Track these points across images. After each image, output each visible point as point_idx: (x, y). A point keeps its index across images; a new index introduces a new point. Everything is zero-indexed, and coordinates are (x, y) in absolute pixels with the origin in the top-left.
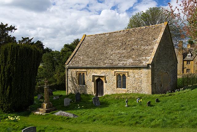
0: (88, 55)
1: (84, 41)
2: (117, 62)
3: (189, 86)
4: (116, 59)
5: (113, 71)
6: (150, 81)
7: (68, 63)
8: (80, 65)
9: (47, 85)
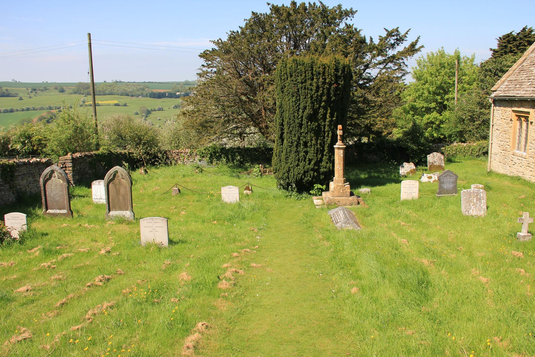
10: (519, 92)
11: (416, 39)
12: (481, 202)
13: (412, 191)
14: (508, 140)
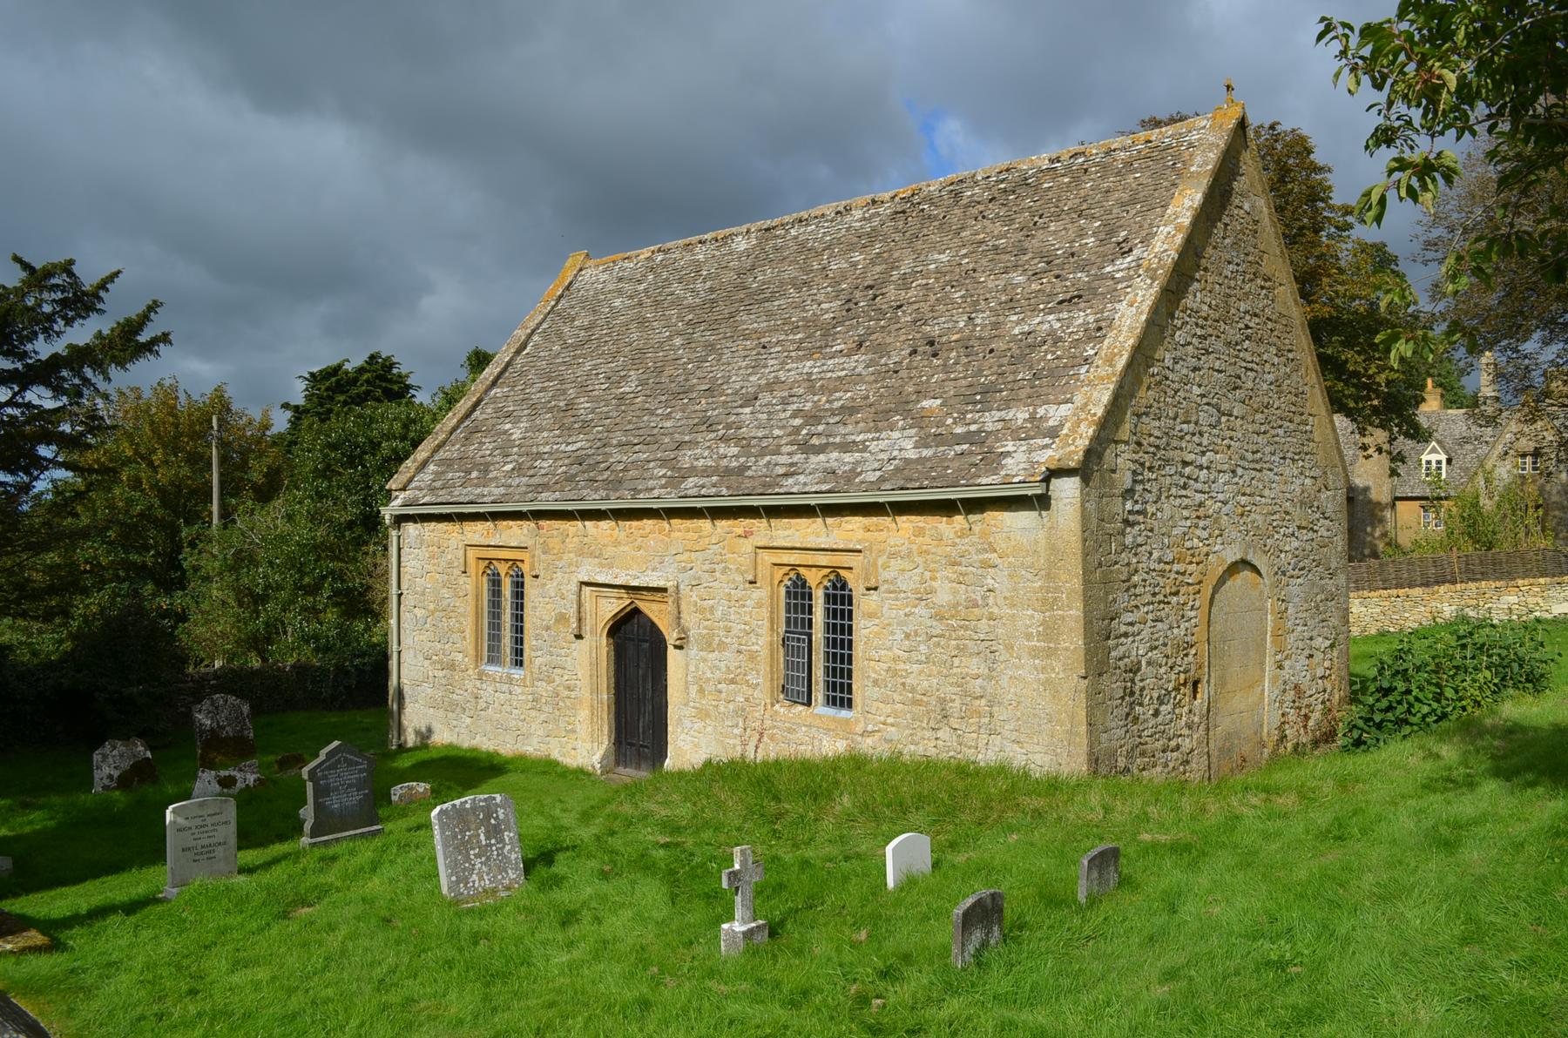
0: (570, 406)
3: (1378, 339)
4: (777, 432)
5: (747, 546)
6: (1073, 641)
7: (410, 480)
11: (141, 309)
12: (502, 841)
13: (213, 841)
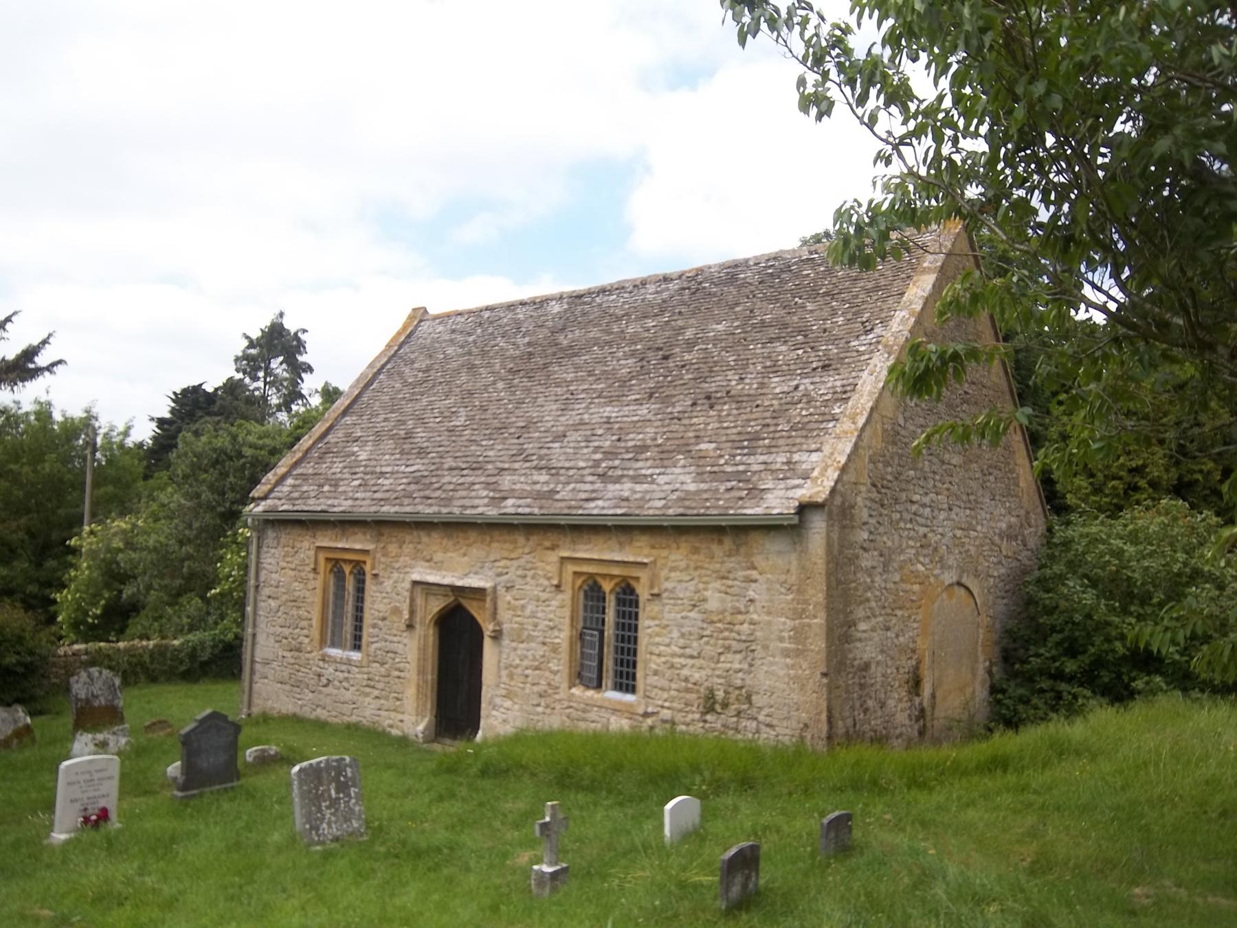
0: (409, 435)
1: (406, 349)
2: (588, 487)
5: (553, 557)
6: (818, 644)
8: (341, 506)
9: (77, 590)
10: (336, 502)
12: (349, 795)
13: (97, 793)
14: (304, 624)
